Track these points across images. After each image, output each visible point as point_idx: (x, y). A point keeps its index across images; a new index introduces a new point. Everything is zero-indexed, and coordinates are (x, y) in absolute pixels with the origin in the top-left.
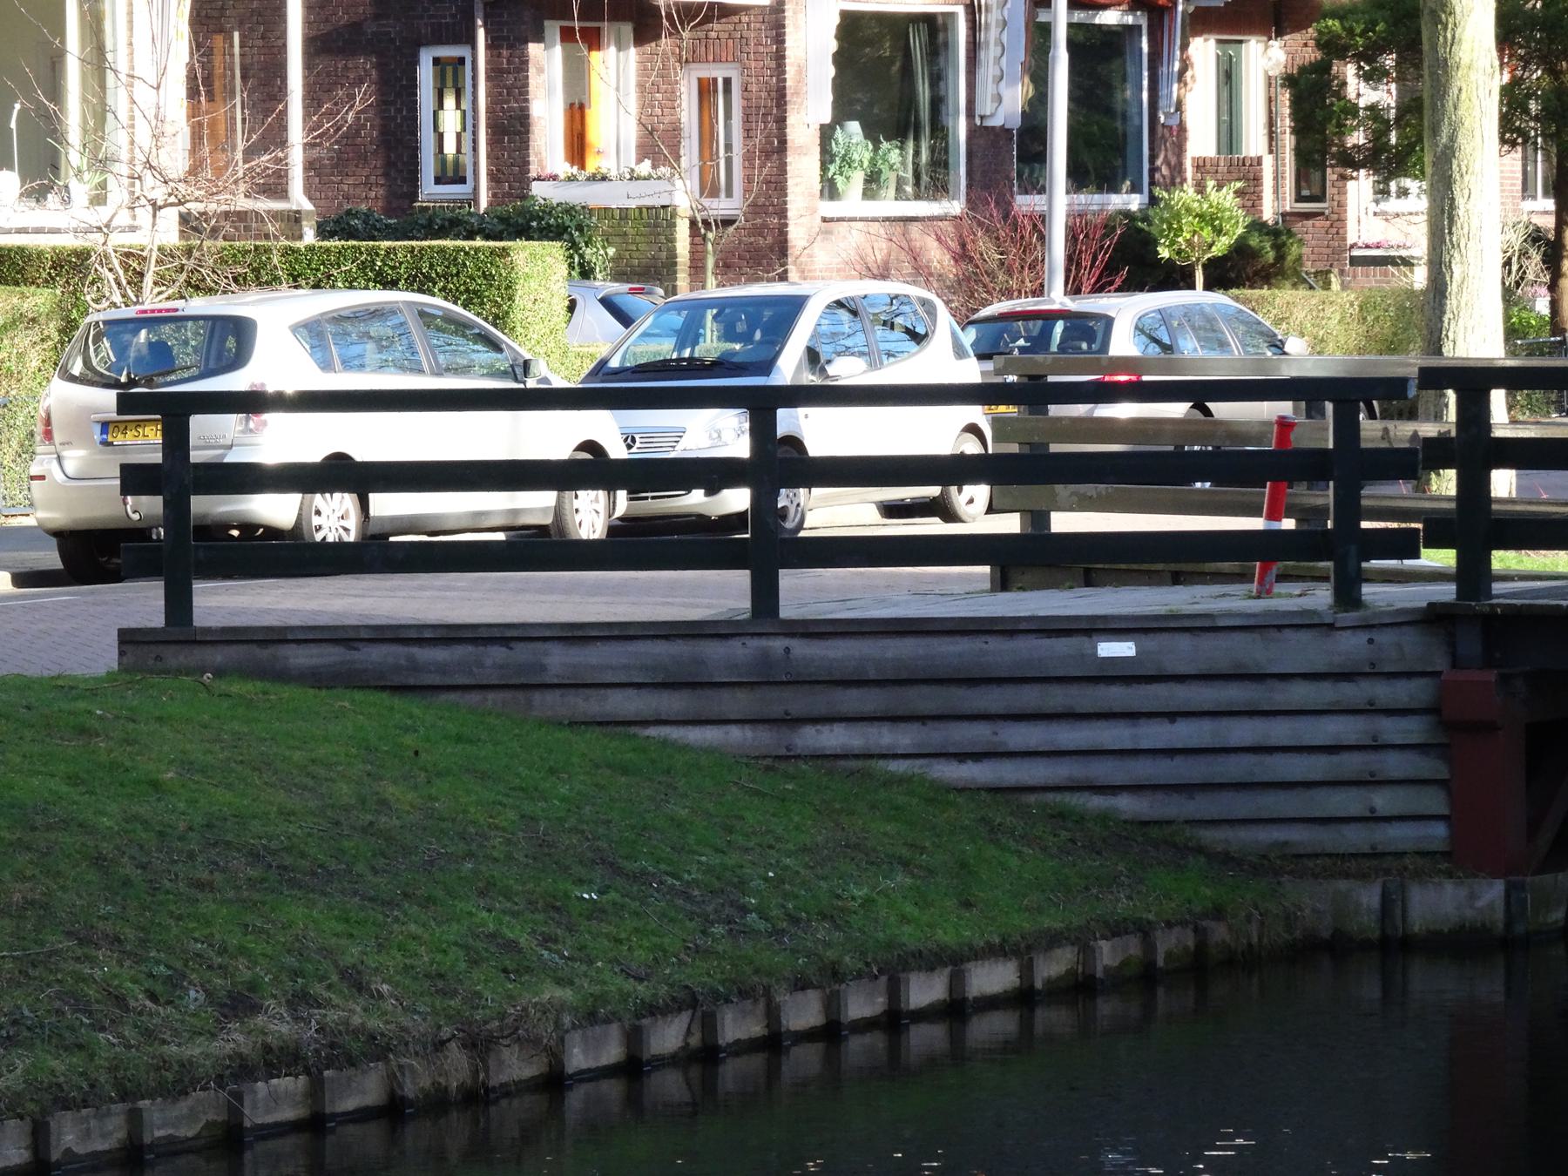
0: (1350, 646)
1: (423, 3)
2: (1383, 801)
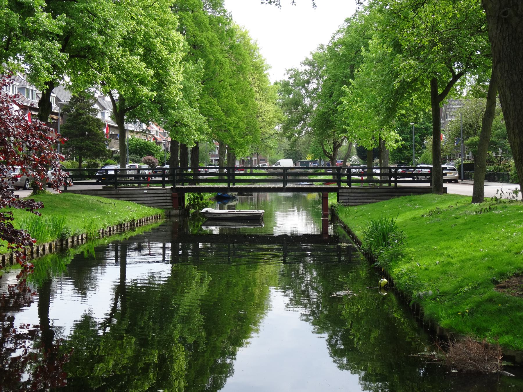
0: (164, 191)
1: (2, 115)
2: (167, 204)
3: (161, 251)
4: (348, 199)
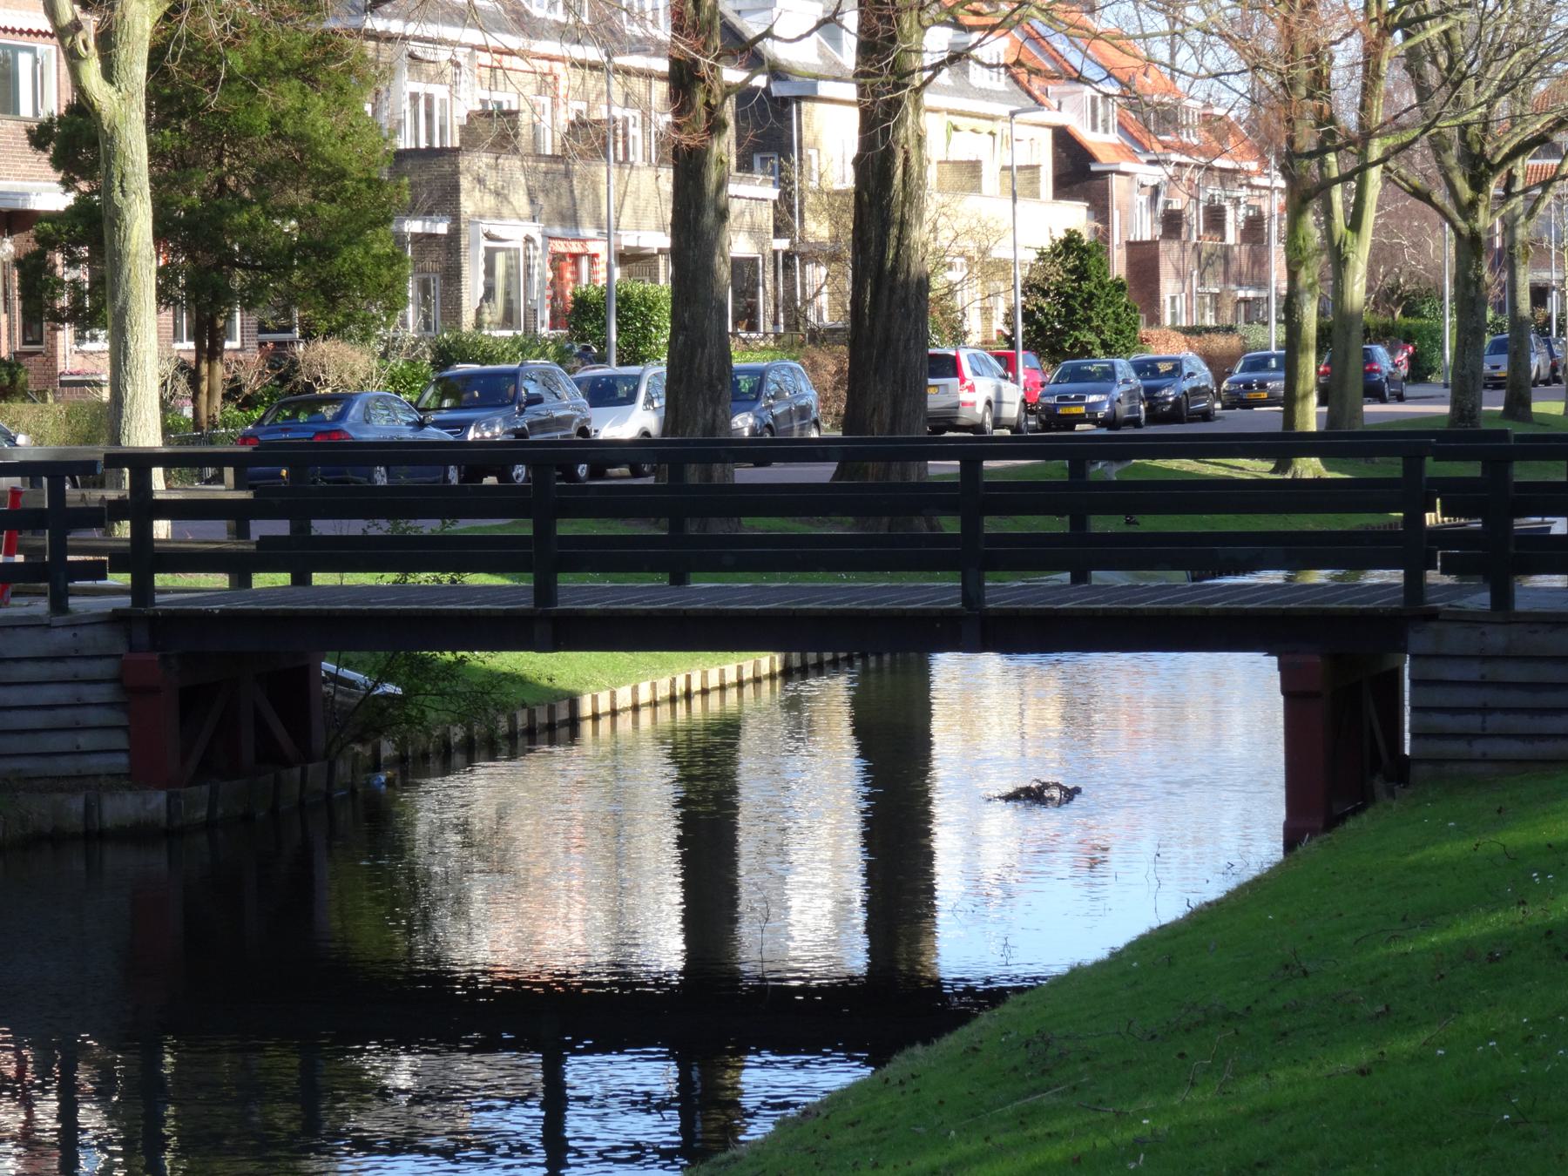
0: (62, 638)
2: (85, 741)
3: (577, 1122)
4: (1485, 710)
